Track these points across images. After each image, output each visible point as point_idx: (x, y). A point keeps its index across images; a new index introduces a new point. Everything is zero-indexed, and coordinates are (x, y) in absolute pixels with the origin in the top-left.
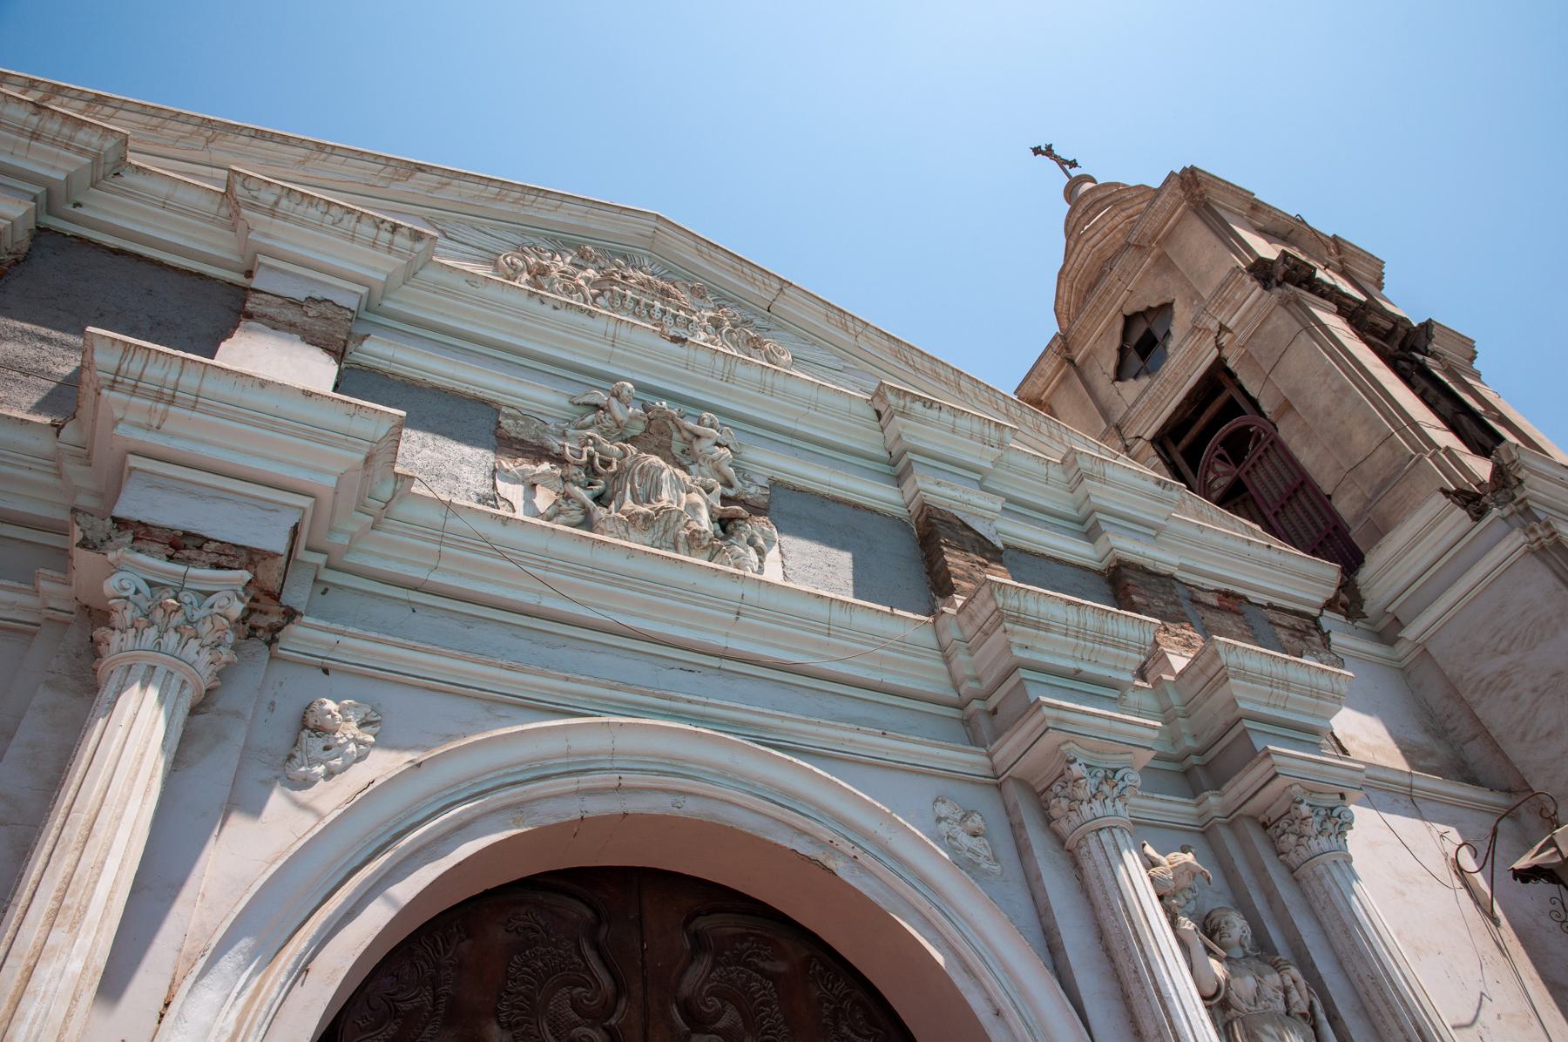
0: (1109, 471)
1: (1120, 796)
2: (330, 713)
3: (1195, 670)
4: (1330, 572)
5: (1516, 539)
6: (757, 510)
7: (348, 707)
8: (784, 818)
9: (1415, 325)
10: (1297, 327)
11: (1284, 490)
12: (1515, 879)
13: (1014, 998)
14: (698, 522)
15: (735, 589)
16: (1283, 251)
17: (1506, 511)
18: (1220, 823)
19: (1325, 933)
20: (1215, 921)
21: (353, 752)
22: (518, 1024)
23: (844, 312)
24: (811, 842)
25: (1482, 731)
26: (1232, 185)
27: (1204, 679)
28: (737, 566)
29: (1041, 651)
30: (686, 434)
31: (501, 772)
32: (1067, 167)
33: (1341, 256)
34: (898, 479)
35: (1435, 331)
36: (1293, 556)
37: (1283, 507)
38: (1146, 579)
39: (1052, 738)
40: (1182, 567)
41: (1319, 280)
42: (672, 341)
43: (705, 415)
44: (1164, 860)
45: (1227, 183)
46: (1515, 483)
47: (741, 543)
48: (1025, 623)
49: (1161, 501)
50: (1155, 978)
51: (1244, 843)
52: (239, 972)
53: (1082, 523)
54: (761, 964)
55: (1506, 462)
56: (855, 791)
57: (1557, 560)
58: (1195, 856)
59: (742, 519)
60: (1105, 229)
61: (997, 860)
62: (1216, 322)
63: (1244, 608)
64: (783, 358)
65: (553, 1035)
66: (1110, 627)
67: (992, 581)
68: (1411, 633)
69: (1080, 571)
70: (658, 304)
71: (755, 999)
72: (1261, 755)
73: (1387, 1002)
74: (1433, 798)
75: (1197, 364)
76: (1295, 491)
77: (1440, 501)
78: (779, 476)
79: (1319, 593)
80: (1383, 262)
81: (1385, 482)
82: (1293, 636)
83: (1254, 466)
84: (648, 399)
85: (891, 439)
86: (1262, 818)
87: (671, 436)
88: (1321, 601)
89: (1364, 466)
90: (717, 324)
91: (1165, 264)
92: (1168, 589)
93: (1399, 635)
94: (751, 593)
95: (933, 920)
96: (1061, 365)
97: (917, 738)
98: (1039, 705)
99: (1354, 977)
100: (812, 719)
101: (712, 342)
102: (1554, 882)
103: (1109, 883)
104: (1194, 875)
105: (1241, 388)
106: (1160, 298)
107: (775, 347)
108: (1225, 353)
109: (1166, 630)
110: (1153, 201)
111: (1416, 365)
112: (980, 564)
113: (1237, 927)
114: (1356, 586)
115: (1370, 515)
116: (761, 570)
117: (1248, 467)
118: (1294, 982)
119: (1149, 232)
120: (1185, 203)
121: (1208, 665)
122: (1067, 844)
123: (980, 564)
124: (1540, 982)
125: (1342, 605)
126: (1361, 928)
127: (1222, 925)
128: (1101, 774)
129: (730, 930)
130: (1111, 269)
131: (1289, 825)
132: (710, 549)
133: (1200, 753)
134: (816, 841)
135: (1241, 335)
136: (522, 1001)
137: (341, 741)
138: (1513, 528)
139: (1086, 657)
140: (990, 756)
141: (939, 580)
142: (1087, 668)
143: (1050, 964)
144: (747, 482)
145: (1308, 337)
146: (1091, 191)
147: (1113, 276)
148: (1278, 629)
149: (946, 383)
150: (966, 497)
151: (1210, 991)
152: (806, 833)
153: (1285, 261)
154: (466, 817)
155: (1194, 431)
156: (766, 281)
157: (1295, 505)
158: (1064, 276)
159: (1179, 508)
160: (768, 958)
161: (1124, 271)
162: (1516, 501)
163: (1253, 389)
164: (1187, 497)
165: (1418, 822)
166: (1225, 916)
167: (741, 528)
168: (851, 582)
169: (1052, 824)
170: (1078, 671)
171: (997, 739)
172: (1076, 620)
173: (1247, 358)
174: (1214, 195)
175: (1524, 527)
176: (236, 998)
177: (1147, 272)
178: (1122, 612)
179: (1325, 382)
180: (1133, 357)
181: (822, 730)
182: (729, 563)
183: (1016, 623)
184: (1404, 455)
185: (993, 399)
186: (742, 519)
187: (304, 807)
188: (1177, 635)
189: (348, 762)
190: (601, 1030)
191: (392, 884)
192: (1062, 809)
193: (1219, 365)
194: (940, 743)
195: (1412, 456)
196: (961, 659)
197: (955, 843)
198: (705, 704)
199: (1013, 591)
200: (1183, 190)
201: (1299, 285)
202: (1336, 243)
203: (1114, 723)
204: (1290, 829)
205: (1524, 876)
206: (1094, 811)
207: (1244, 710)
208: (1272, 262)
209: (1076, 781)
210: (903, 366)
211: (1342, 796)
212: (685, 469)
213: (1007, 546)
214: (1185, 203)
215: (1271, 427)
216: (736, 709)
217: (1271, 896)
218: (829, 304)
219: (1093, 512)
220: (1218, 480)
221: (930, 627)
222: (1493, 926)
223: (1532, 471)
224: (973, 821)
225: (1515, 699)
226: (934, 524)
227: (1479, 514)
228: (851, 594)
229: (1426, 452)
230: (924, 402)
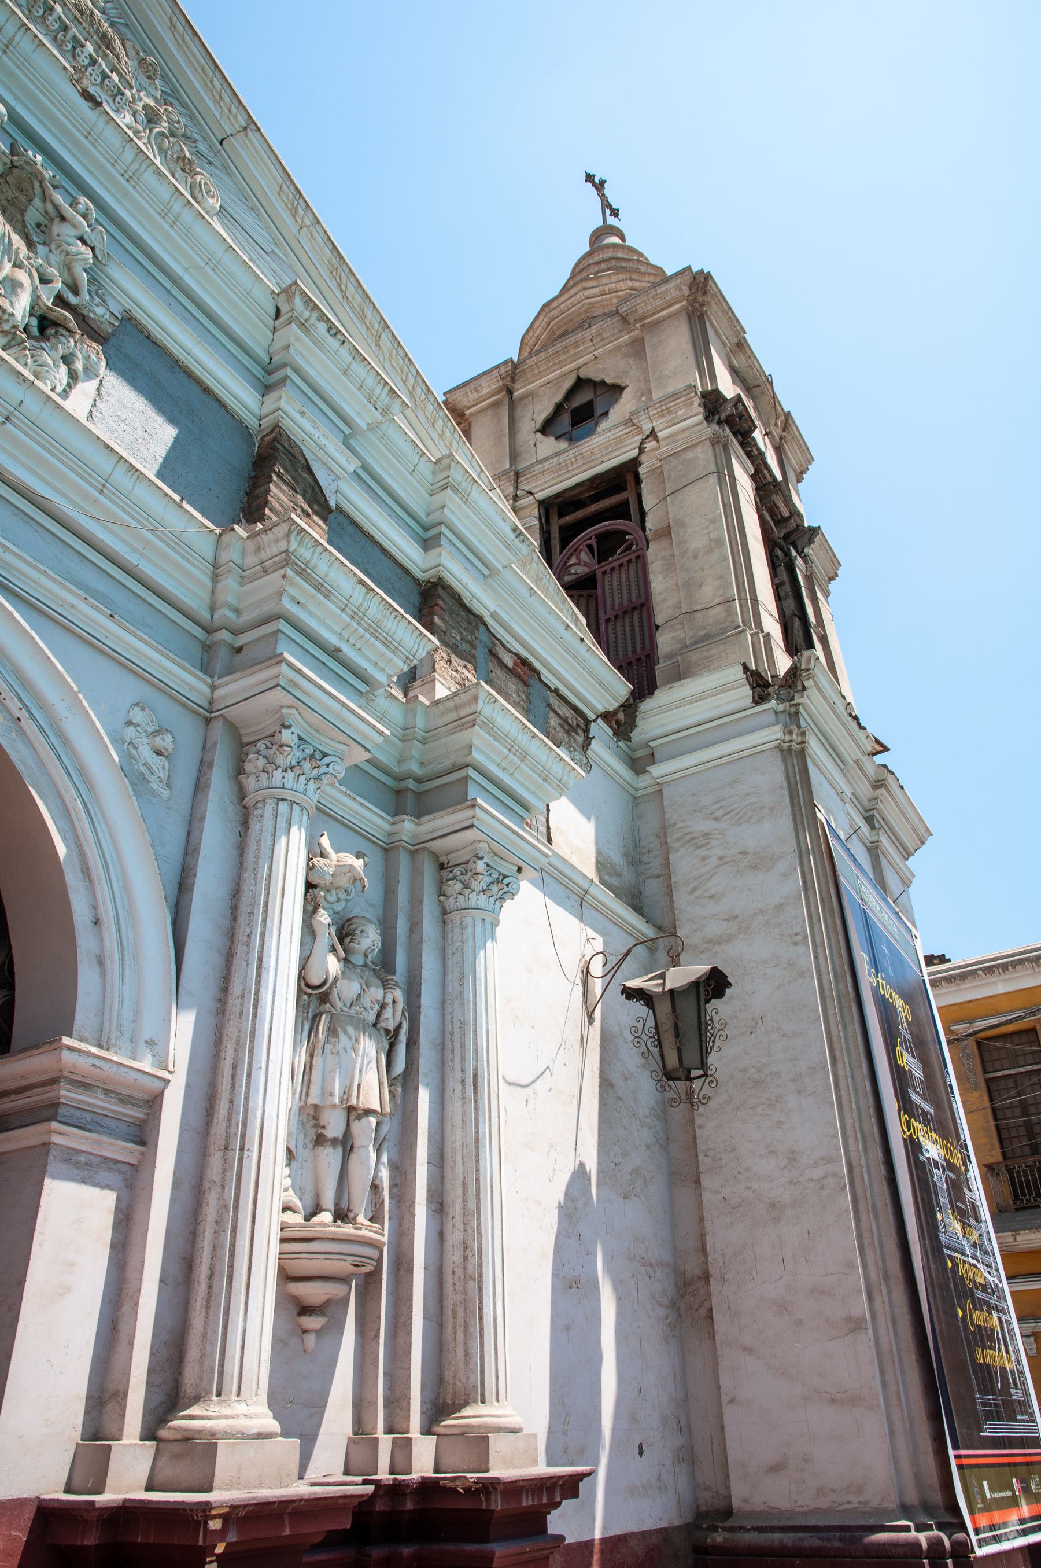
0: (475, 494)
1: (318, 778)
3: (450, 704)
4: (622, 688)
5: (776, 733)
6: (92, 331)
9: (806, 525)
10: (712, 467)
11: (625, 603)
12: (622, 993)
13: (121, 916)
14: (11, 303)
15: (16, 392)
16: (739, 396)
17: (781, 707)
18: (404, 847)
19: (444, 974)
20: (353, 927)
23: (301, 195)
25: (666, 874)
26: (733, 312)
27: (454, 716)
28: (37, 376)
29: (311, 614)
30: (50, 208)
32: (608, 212)
33: (784, 434)
34: (266, 389)
35: (817, 539)
36: (597, 658)
37: (616, 617)
38: (456, 608)
39: (277, 697)
40: (494, 616)
41: (754, 439)
42: (82, 95)
43: (83, 200)
44: (333, 855)
45: (730, 308)
46: (800, 688)
47: (53, 353)
48: (307, 578)
49: (508, 547)
50: (263, 948)
51: (416, 873)
53: (426, 529)
55: (802, 668)
56: (50, 654)
57: (793, 765)
58: (365, 865)
59: (68, 330)
60: (606, 288)
61: (169, 786)
62: (650, 426)
63: (533, 681)
64: (211, 201)
66: (389, 624)
67: (294, 522)
68: (657, 771)
69: (399, 571)
70: (90, 48)
72: (468, 803)
73: (463, 1046)
74: (599, 909)
75: (617, 453)
76: (634, 609)
77: (738, 673)
78: (137, 314)
79: (604, 703)
80: (813, 459)
81: (707, 637)
82: (562, 726)
83: (613, 569)
84: (22, 141)
85: (279, 344)
86: (443, 859)
87: (30, 201)
88: (601, 709)
89: (699, 615)
90: (152, 118)
91: (638, 349)
92: (470, 628)
93: (647, 768)
94: (33, 406)
96: (499, 391)
97: (146, 637)
98: (279, 660)
99: (448, 1017)
100: (39, 565)
101: (136, 132)
102: (648, 1006)
103: (265, 850)
104: (355, 880)
105: (639, 496)
106: (617, 377)
107: (206, 183)
108: (643, 458)
109: (449, 661)
110: (655, 285)
111: (788, 558)
112: (303, 511)
113: (369, 939)
114: (637, 711)
115: (680, 658)
116: (65, 394)
117: (608, 568)
118: (394, 1002)
119: (640, 311)
120: (684, 303)
121: (463, 705)
122: (246, 800)
123: (303, 511)
124: (597, 1076)
125: (617, 722)
126: (474, 981)
127: (356, 932)
128: (309, 751)
130: (590, 326)
131: (462, 874)
132: (10, 337)
133: (419, 780)
135: (665, 449)
138: (777, 723)
139: (352, 641)
140: (213, 688)
141: (254, 504)
142: (347, 651)
143: (173, 899)
144: (98, 300)
145: (716, 480)
146: (615, 246)
147: (588, 334)
148: (552, 714)
149: (368, 328)
150: (323, 441)
151: (315, 981)
153: (735, 405)
155: (580, 514)
156: (234, 109)
157: (627, 621)
158: (547, 310)
159: (523, 565)
161: (600, 334)
162: (793, 702)
163: (648, 503)
164: (536, 559)
165: (575, 921)
166: (364, 925)
167: (61, 338)
168: (161, 460)
169: (241, 777)
170: (338, 650)
171: (229, 674)
172: (360, 601)
173: (658, 472)
174: (713, 314)
175: (786, 726)
177: (618, 348)
178: (408, 616)
179: (708, 527)
180: (566, 419)
182: (26, 364)
183: (299, 574)
184: (733, 621)
185: (406, 370)
186: (68, 330)
188: (456, 671)
192: (256, 767)
193: (633, 464)
194: (168, 652)
195: (739, 627)
196: (230, 583)
197: (134, 752)
199: (312, 543)
200: (690, 289)
201: (735, 434)
202: (787, 419)
203: (345, 711)
204: (461, 877)
205: (630, 994)
206: (479, 902)
207: (475, 759)
208: (725, 400)
209: (281, 746)
210: (333, 286)
211: (520, 870)
212: (30, 245)
213: (339, 509)
214: (684, 303)
215: (645, 542)
217: (415, 926)
218: (289, 176)
219: (441, 523)
220: (576, 567)
221: (213, 539)
222: (587, 1023)
223: (816, 685)
224: (163, 740)
225: (704, 859)
226: (277, 450)
227: (760, 699)
228: (155, 471)
229: (751, 629)
230: (331, 327)
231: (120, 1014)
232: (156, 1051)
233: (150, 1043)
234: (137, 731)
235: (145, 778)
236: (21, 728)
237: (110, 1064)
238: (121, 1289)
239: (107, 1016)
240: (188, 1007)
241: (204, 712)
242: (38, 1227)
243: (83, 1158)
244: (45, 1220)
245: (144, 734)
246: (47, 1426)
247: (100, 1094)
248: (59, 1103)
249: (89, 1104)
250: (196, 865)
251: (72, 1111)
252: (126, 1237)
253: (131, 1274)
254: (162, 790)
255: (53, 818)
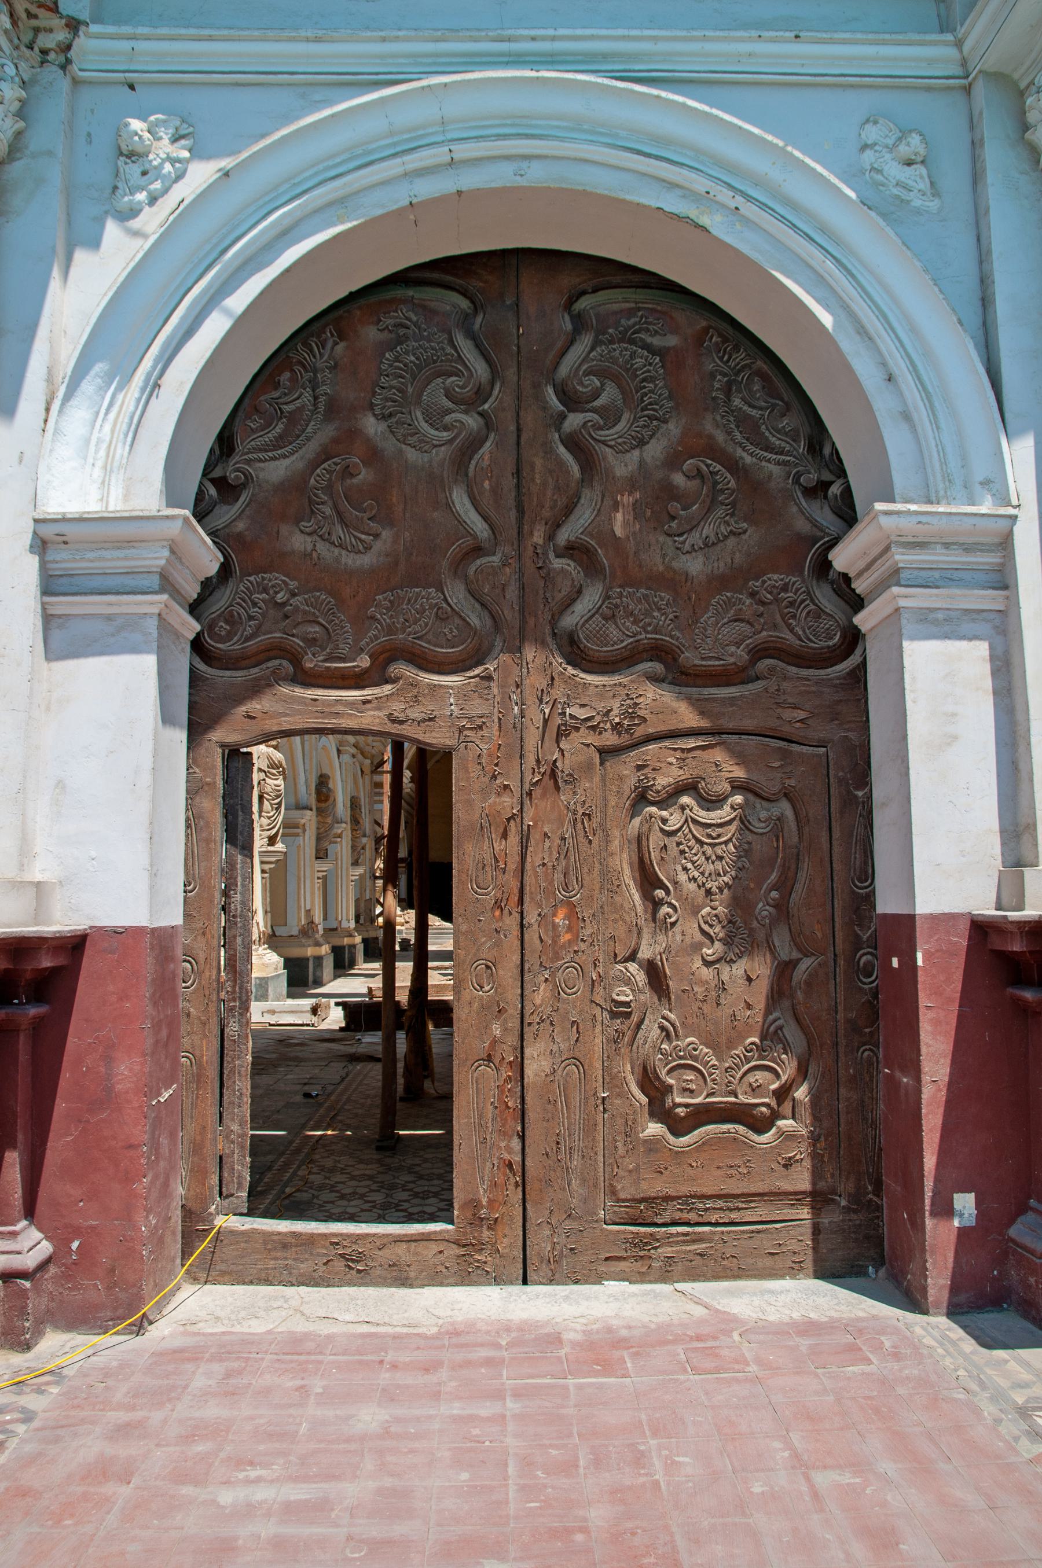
2: (136, 134)
7: (157, 123)
8: (650, 170)
21: (170, 173)
22: (390, 415)
24: (684, 196)
31: (321, 167)
52: (102, 393)
54: (649, 340)
56: (739, 123)
61: (936, 193)
65: (426, 422)
71: (637, 376)
95: (826, 276)
100: (695, 33)
129: (616, 307)
134: (688, 193)
136: (394, 394)
137: (155, 163)
140: (959, 44)
152: (677, 186)
154: (286, 222)
160: (656, 332)
176: (106, 414)
181: (709, 47)
187: (136, 234)
189: (167, 184)
190: (476, 416)
191: (224, 299)
194: (881, 36)
197: (879, 177)
198: (553, 39)
216: (592, 38)
224: (908, 144)
231: (944, 463)
232: (994, 490)
233: (986, 483)
234: (876, 151)
235: (902, 201)
236: (743, 216)
237: (938, 517)
238: (1014, 732)
239: (929, 470)
240: (1021, 432)
241: (957, 81)
242: (907, 686)
243: (940, 616)
244: (914, 679)
245: (884, 150)
246: (963, 856)
247: (939, 549)
248: (899, 569)
249: (933, 562)
250: (992, 270)
251: (916, 572)
252: (1010, 683)
253: (1020, 717)
254: (927, 204)
255: (808, 292)
